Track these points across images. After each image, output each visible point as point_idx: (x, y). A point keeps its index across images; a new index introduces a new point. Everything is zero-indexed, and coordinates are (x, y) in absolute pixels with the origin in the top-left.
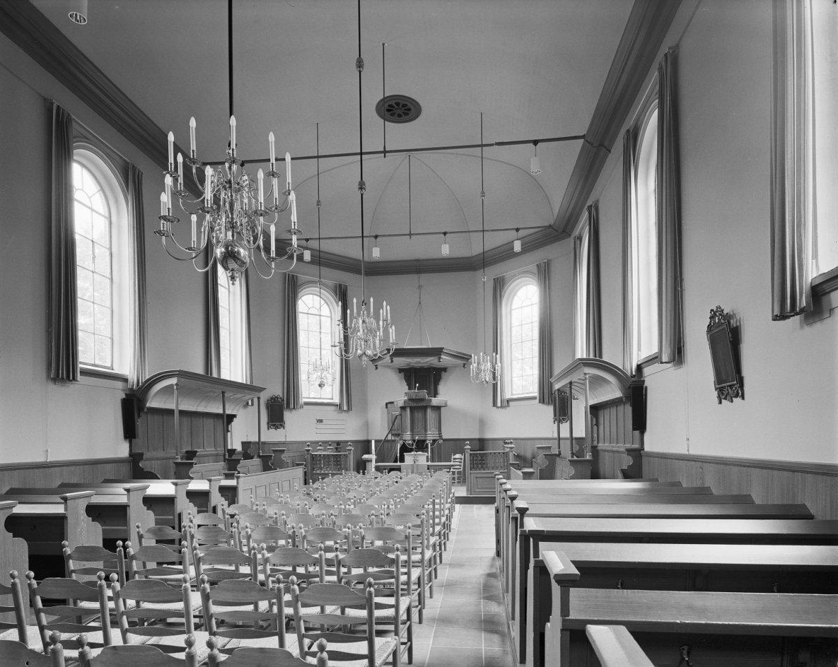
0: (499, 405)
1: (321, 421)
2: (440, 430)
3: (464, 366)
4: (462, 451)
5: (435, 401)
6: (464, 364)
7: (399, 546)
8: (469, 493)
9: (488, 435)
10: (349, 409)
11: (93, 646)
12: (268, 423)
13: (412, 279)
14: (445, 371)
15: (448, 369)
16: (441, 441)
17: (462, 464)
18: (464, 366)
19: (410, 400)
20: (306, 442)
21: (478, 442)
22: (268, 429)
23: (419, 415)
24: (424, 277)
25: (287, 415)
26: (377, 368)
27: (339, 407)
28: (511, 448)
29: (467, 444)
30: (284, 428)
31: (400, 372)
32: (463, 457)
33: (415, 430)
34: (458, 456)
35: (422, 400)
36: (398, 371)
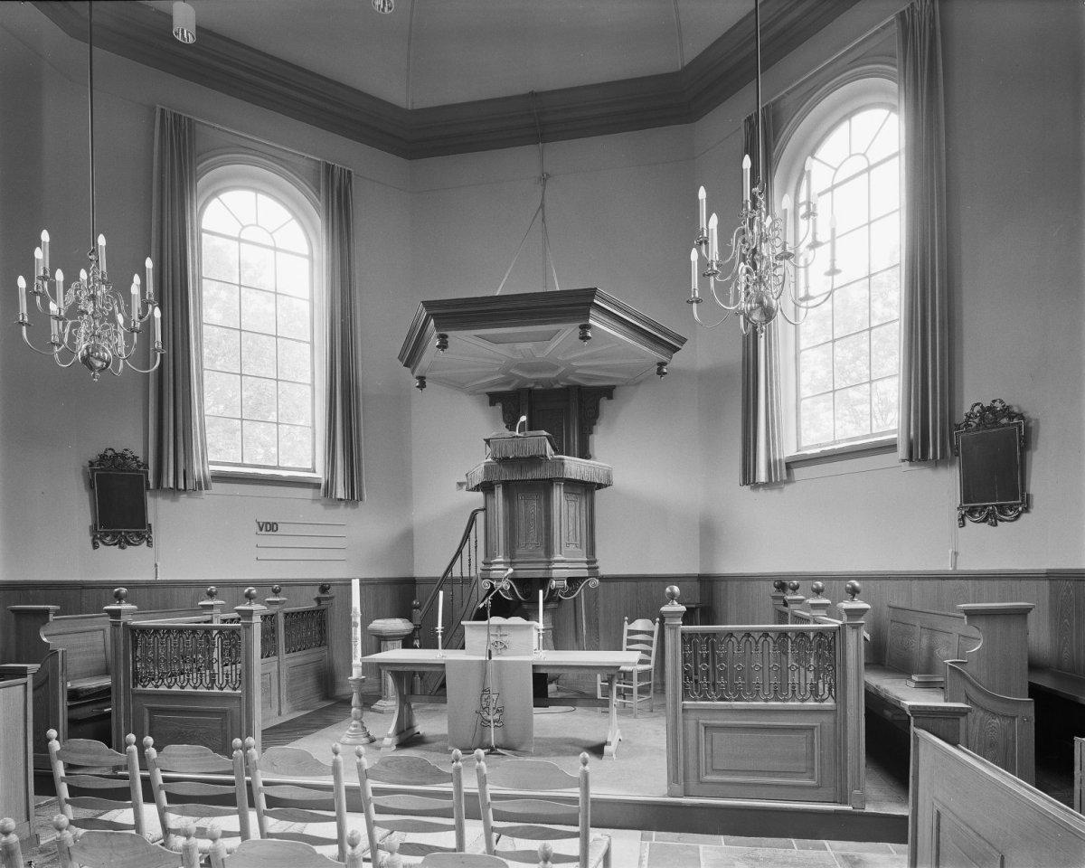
0: (762, 476)
1: (271, 527)
2: (591, 550)
3: (660, 373)
4: (652, 612)
5: (574, 467)
6: (662, 364)
7: (676, 589)
8: (678, 788)
9: (726, 567)
10: (354, 497)
11: (226, 834)
12: (94, 530)
13: (519, 162)
14: (610, 397)
15: (616, 392)
16: (595, 583)
17: (654, 649)
18: (660, 373)
19: (504, 461)
20: (204, 584)
21: (697, 585)
22: (95, 546)
23: (529, 507)
24: (562, 154)
25: (159, 510)
26: (422, 385)
27: (326, 491)
28: (853, 613)
29: (672, 596)
30: (149, 544)
31: (492, 403)
32: (656, 628)
33: (518, 552)
34: (640, 624)
35: (536, 460)
36: (487, 399)
